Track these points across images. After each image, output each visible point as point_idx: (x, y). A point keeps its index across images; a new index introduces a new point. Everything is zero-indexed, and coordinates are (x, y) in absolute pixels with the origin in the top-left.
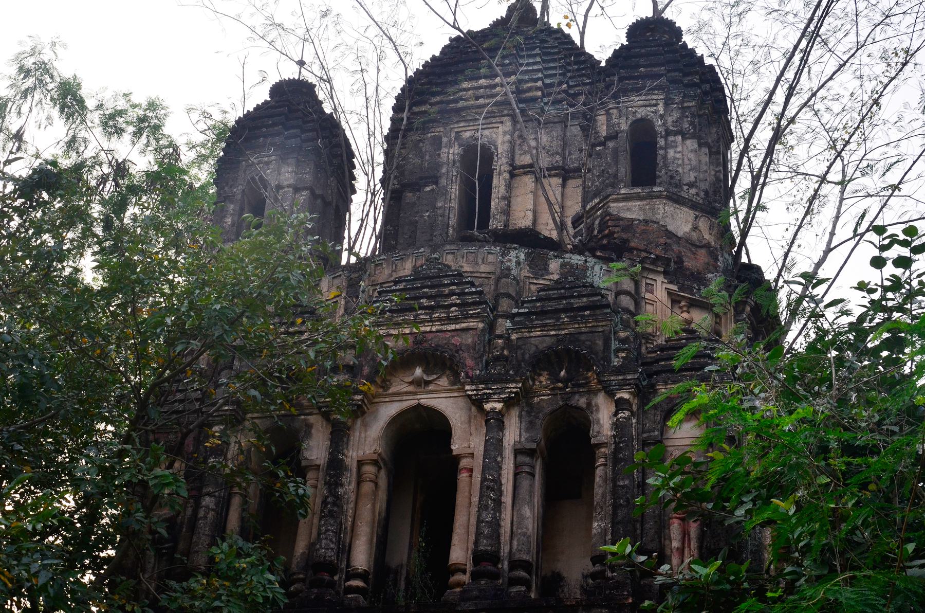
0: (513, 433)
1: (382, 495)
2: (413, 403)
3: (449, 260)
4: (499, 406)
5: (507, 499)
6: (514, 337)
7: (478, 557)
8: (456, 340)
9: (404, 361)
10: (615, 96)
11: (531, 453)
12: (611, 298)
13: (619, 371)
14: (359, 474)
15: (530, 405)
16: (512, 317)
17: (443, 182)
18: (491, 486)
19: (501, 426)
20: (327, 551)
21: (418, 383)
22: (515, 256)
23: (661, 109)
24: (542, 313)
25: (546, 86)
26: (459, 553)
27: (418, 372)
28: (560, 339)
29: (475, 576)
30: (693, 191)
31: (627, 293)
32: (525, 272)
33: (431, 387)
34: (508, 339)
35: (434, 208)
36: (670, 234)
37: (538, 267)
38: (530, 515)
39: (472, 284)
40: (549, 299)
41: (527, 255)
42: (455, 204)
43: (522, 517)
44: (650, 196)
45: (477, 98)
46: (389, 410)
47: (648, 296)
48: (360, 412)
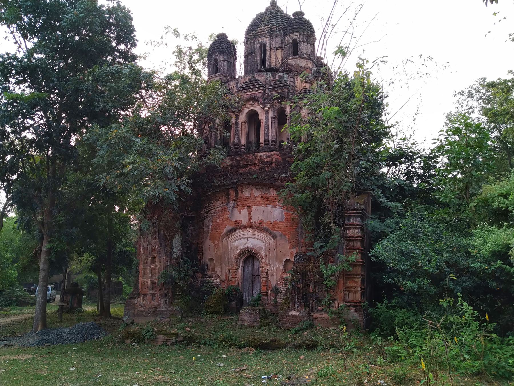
0: (270, 114)
1: (247, 128)
2: (251, 109)
3: (256, 76)
4: (267, 109)
5: (270, 128)
7: (265, 141)
8: (258, 95)
9: (248, 100)
10: (289, 34)
11: (274, 118)
12: (288, 83)
14: (242, 125)
15: (273, 108)
16: (269, 89)
17: (256, 53)
18: (267, 126)
19: (268, 113)
20: (237, 141)
21: (251, 105)
22: (270, 74)
23: (298, 36)
25: (277, 26)
26: (261, 140)
27: (251, 102)
30: (306, 55)
31: (292, 82)
32: (271, 78)
33: (254, 105)
35: (255, 60)
36: (301, 67)
37: (274, 76)
38: (275, 131)
39: (260, 82)
41: (272, 74)
42: (259, 58)
45: (262, 32)
46: (246, 111)
47: (296, 81)
48: (240, 112)
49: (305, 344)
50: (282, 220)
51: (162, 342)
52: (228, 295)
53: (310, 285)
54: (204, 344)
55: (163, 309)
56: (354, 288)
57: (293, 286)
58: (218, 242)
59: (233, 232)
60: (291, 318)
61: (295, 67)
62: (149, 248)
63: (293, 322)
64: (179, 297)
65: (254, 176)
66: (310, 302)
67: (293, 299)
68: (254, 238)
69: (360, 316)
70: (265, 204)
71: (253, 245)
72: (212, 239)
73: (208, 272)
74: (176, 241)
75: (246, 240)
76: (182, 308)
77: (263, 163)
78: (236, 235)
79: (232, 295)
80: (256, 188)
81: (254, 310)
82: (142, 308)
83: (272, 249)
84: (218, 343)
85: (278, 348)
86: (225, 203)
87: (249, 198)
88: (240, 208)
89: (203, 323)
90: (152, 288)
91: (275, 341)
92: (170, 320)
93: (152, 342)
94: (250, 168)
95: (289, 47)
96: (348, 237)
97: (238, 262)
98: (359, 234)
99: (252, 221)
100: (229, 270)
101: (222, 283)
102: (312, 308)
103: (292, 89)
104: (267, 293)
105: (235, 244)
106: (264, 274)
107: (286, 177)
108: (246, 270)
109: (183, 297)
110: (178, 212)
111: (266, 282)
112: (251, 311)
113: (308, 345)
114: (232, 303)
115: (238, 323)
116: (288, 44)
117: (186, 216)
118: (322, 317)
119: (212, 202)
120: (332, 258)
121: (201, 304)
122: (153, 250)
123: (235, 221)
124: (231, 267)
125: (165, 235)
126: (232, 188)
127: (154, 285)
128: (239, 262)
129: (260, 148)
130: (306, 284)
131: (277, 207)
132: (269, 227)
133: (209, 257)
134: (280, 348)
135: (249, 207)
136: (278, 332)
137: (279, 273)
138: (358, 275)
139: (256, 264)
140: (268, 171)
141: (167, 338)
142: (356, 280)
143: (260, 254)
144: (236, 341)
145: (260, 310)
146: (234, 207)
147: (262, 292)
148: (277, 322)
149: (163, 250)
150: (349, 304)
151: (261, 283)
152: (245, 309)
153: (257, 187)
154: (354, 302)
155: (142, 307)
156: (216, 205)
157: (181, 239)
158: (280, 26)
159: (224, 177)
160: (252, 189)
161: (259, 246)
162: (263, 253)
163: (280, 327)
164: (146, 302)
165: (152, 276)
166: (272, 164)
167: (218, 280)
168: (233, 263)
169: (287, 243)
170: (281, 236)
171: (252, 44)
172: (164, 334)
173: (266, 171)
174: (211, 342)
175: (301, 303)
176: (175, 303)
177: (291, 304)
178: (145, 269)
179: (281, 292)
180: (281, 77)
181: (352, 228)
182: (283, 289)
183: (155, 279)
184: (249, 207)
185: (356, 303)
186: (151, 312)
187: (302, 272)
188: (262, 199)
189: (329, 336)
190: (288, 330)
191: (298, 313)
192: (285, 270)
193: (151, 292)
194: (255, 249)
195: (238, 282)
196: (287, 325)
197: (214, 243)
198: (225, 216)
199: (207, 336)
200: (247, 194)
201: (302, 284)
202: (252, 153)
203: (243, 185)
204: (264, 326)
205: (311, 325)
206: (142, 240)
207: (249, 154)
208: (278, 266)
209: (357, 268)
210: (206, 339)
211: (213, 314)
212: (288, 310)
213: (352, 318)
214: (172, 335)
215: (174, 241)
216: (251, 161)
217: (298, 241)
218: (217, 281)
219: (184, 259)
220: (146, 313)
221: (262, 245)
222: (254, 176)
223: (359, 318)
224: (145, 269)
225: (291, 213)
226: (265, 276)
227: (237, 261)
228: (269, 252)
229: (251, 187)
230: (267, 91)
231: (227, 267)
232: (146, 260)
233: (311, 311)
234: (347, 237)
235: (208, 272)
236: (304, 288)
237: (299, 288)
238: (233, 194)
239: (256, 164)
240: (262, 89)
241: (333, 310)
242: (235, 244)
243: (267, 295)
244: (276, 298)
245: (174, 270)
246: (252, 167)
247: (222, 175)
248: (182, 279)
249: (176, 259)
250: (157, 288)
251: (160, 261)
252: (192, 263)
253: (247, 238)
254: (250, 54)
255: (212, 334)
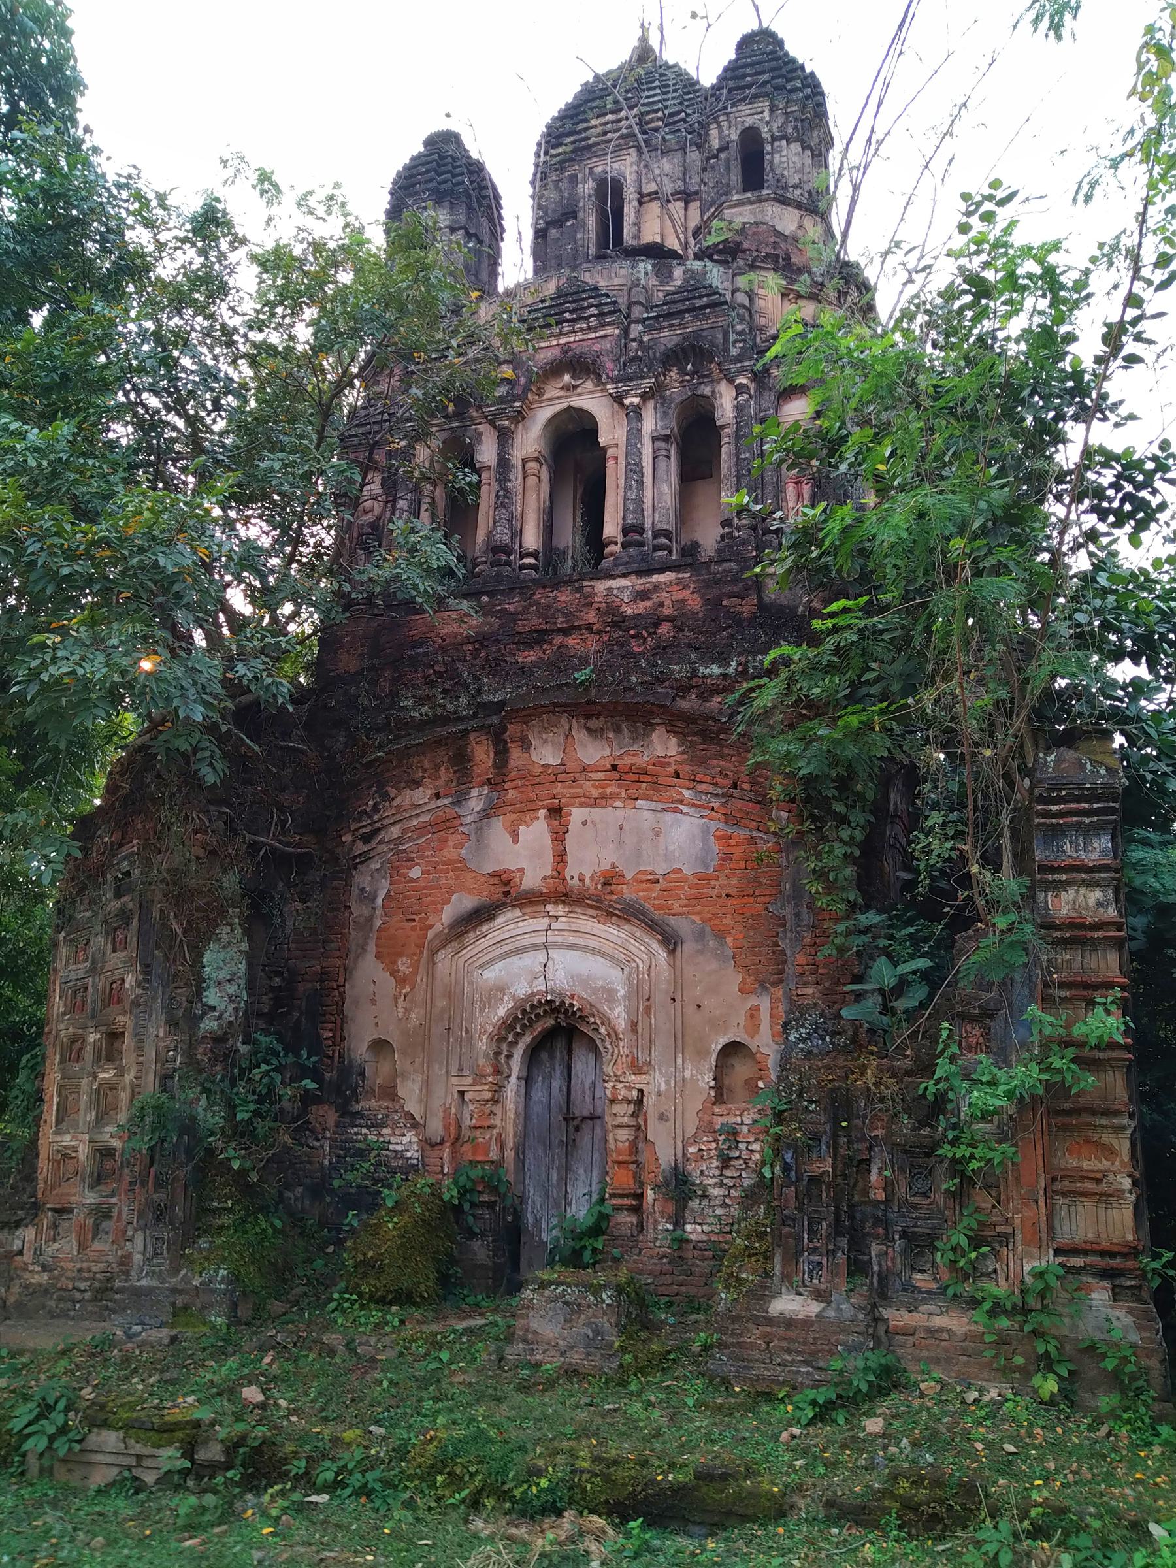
2: (565, 405)
3: (586, 277)
4: (636, 400)
5: (648, 479)
6: (645, 339)
7: (626, 531)
8: (597, 347)
9: (554, 370)
11: (666, 439)
12: (728, 297)
13: (737, 359)
15: (663, 398)
17: (581, 215)
18: (634, 469)
20: (503, 536)
21: (567, 388)
23: (766, 115)
24: (669, 315)
26: (611, 528)
27: (567, 378)
28: (685, 337)
29: (625, 546)
30: (798, 192)
32: (653, 281)
33: (579, 390)
34: (641, 341)
35: (575, 240)
36: (778, 234)
37: (664, 275)
39: (607, 296)
40: (674, 302)
41: (654, 266)
42: (592, 235)
43: (661, 494)
44: (760, 200)
45: (605, 133)
46: (544, 414)
47: (760, 291)
48: (519, 417)
49: (894, 1497)
50: (707, 866)
51: (115, 1471)
52: (458, 1209)
53: (868, 1162)
54: (332, 1487)
55: (143, 1283)
56: (1098, 1181)
57: (786, 1168)
58: (415, 968)
59: (481, 924)
60: (781, 1331)
61: (754, 234)
62: (96, 987)
63: (789, 1351)
64: (225, 1220)
65: (580, 676)
66: (875, 1249)
67: (789, 1235)
68: (579, 948)
69: (1139, 1328)
70: (629, 797)
71: (576, 978)
72: (388, 956)
73: (364, 1104)
74: (222, 955)
75: (541, 956)
76: (235, 1278)
77: (619, 621)
78: (496, 936)
79: (473, 1205)
80: (589, 730)
81: (588, 1287)
82: (45, 1276)
83: (660, 998)
84: (411, 1478)
85: (745, 1519)
86: (446, 796)
87: (556, 774)
88: (514, 816)
89: (332, 1352)
90: (98, 1179)
91: (724, 1477)
92: (174, 1340)
93: (61, 1473)
94: (562, 646)
95: (727, 161)
96: (1056, 928)
97: (502, 1058)
98: (1111, 913)
99: (568, 873)
100: (462, 1093)
101: (429, 1152)
102: (883, 1278)
103: (742, 319)
104: (640, 1197)
105: (491, 975)
106: (623, 1112)
107: (724, 676)
108: (538, 1094)
109: (244, 1221)
110: (234, 831)
111: (634, 1148)
112: (572, 1294)
113: (909, 1505)
114: (476, 1245)
115: (513, 1352)
116: (724, 148)
117: (274, 850)
118: (941, 1330)
119: (392, 792)
120: (977, 1031)
121: (331, 1249)
122: (113, 996)
123: (493, 875)
124: (469, 1080)
125: (165, 926)
126: (480, 729)
127: (109, 1165)
128: (509, 1057)
129: (606, 564)
130: (851, 1159)
131: (684, 809)
132: (646, 899)
133: (370, 1035)
134: (753, 1519)
135: (556, 812)
136: (720, 1408)
137: (696, 1104)
138: (1117, 1113)
139: (582, 1065)
140: (643, 653)
141: (139, 1448)
142: (1107, 1138)
143: (606, 1021)
144: (504, 1471)
145: (619, 1289)
146: (486, 815)
147: (613, 1195)
148: (706, 1348)
149: (154, 999)
150: (1078, 1262)
151: (605, 1150)
152: (543, 1285)
153: (593, 723)
154: (1102, 1253)
155: (45, 1268)
156: (407, 802)
157: (245, 946)
158: (679, 112)
159: (448, 685)
160: (569, 735)
161: (599, 983)
162: (619, 1016)
163: (726, 1383)
164: (65, 1247)
165: (100, 1121)
166: (657, 625)
167: (410, 1137)
168: (481, 1062)
169: (731, 970)
170: (700, 936)
171: (564, 185)
172: (128, 1427)
173: (634, 656)
174: (370, 1476)
175: (830, 1253)
176: (200, 1250)
177: (778, 1259)
178: (67, 1088)
179: (704, 1196)
180: (690, 275)
181: (1075, 881)
182: (711, 1181)
183: (110, 1136)
184: (556, 812)
185: (1112, 1255)
186: (88, 1295)
187: (834, 1100)
188: (616, 774)
189: (1010, 1448)
190: (768, 1396)
191: (814, 1308)
192: (721, 1093)
193: (91, 1198)
194: (580, 998)
195: (502, 1149)
196: (761, 1370)
197: (394, 973)
198: (449, 853)
199: (349, 1435)
200: (546, 754)
201: (835, 1159)
202: (570, 582)
203: (526, 713)
204: (642, 1371)
205: (886, 1371)
206: (63, 952)
207: (557, 584)
208: (687, 1074)
209: (1110, 1076)
210: (346, 1455)
211: (383, 1302)
212: (763, 1293)
213: (1098, 1336)
214: (167, 1430)
215: (208, 957)
216: (565, 615)
217: (780, 959)
218: (407, 1143)
219: (256, 1042)
220: (60, 1299)
221: (615, 977)
222: (580, 676)
223: (1134, 1337)
224: (67, 1088)
225: (744, 834)
226: (626, 1120)
227: (497, 1054)
228: (648, 1010)
229: (564, 721)
230: (636, 329)
231: (455, 1080)
232: (78, 1045)
233: (882, 1294)
234: (1056, 928)
235: (364, 1104)
236: (840, 1180)
237: (815, 1180)
238: (482, 754)
239: (589, 627)
240: (613, 323)
241: (999, 1289)
242: (491, 975)
243: (637, 1210)
244: (679, 1222)
245: (206, 1090)
246: (572, 641)
247: (440, 675)
248: (240, 1133)
249: (219, 1039)
250: (120, 1179)
251: (139, 1048)
252: (291, 1059)
253: (546, 946)
254: (558, 223)
255: (377, 1423)
